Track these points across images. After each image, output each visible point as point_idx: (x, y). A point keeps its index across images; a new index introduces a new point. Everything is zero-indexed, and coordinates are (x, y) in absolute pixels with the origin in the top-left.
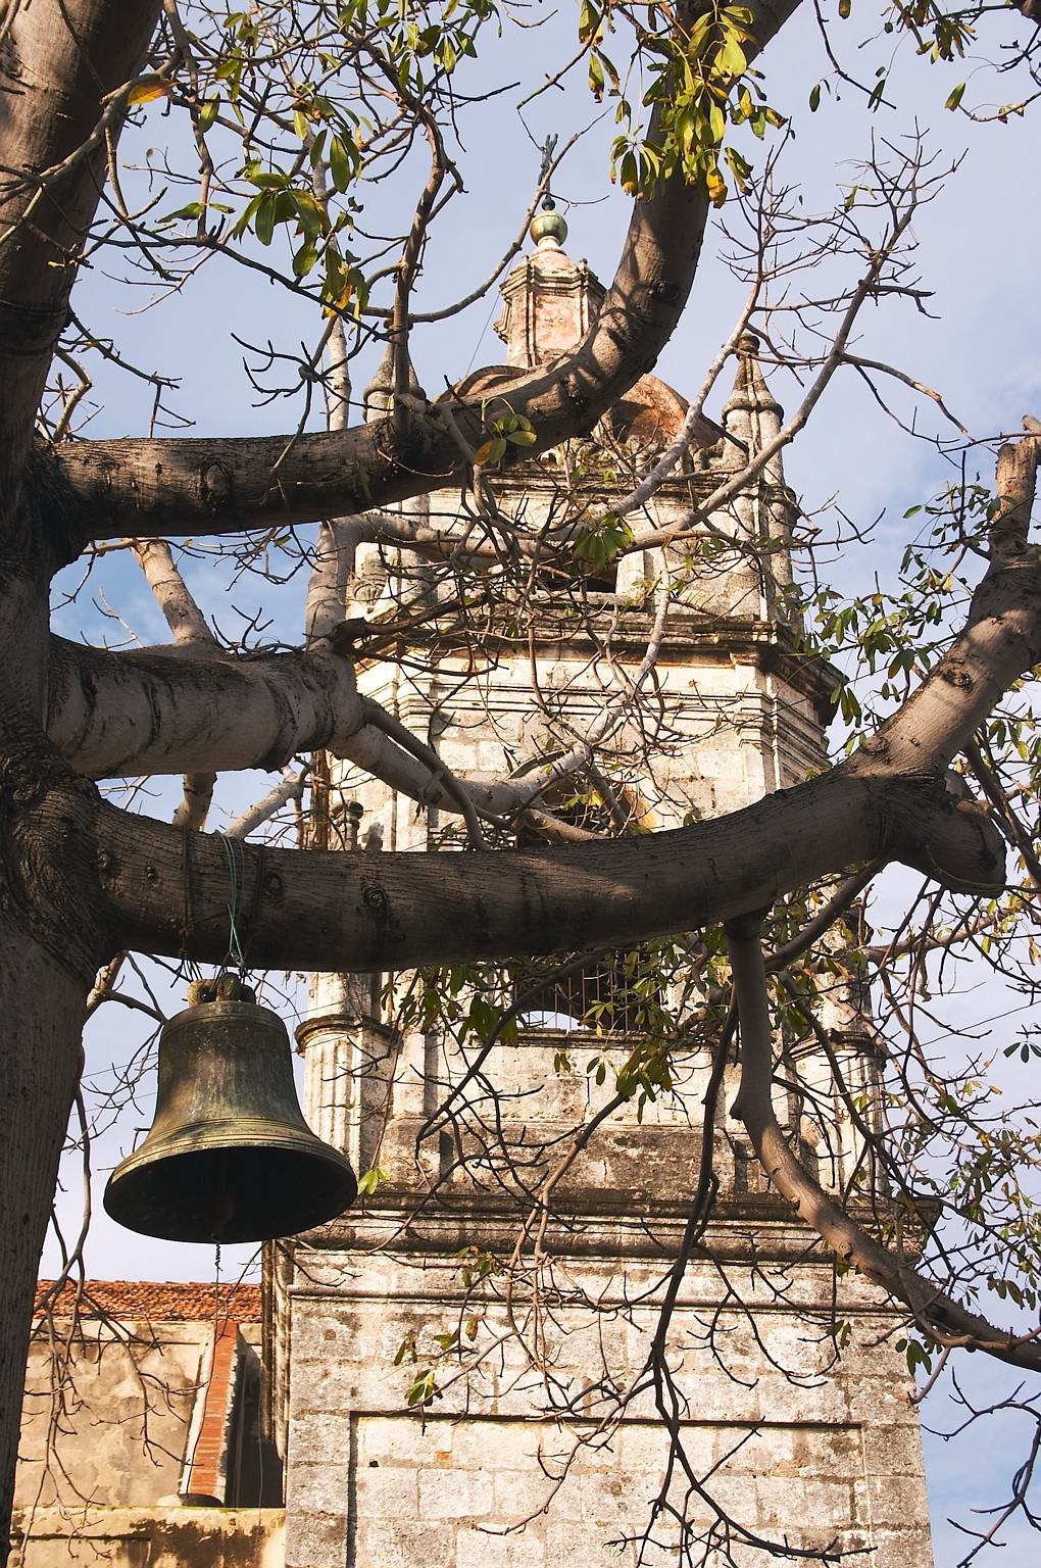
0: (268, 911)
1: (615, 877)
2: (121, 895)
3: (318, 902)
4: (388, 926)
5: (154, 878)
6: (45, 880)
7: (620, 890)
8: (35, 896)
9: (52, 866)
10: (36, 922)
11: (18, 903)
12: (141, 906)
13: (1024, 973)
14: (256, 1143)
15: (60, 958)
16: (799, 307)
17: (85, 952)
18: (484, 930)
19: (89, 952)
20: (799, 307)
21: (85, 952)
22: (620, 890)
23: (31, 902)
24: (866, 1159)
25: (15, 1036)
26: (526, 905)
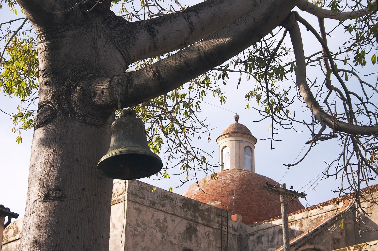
0: (130, 90)
1: (225, 37)
2: (98, 101)
3: (142, 82)
4: (161, 80)
5: (103, 94)
6: (78, 105)
7: (227, 40)
8: (76, 110)
9: (79, 102)
10: (78, 117)
11: (73, 114)
12: (102, 102)
13: (134, 8)
14: (109, 157)
15: (85, 123)
16: (361, 122)
17: (93, 118)
18: (189, 69)
19: (95, 118)
20: (361, 122)
21: (93, 118)
22: (227, 40)
23: (76, 112)
24: (366, 26)
25: (73, 147)
26: (200, 57)
